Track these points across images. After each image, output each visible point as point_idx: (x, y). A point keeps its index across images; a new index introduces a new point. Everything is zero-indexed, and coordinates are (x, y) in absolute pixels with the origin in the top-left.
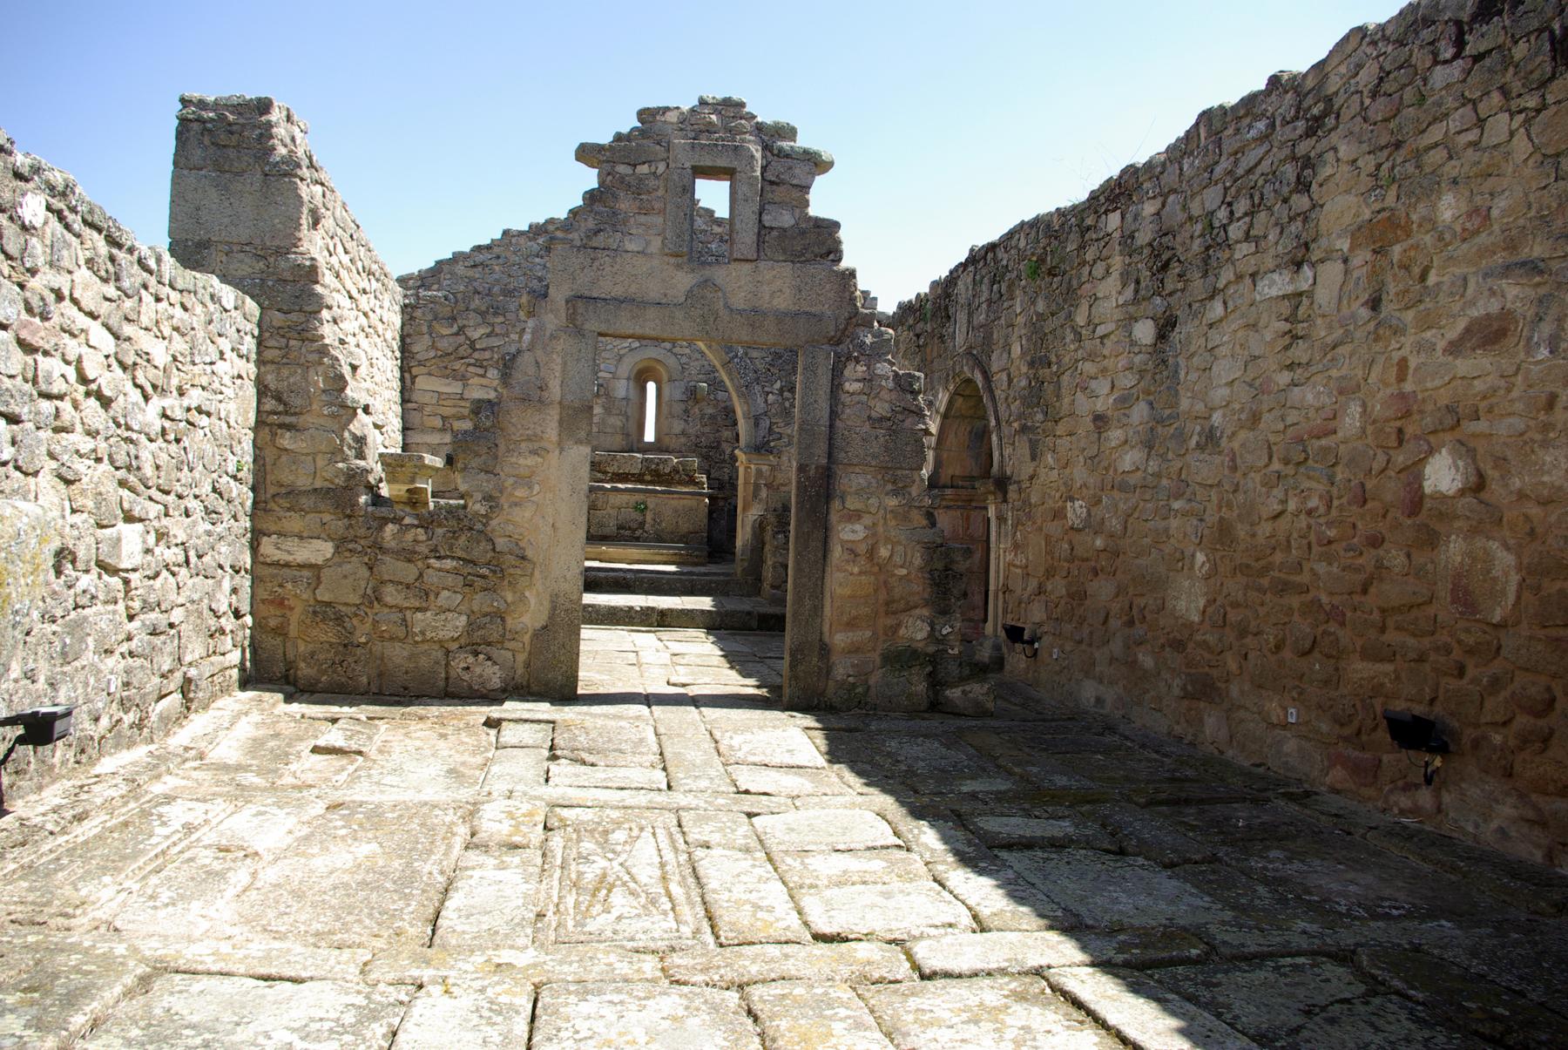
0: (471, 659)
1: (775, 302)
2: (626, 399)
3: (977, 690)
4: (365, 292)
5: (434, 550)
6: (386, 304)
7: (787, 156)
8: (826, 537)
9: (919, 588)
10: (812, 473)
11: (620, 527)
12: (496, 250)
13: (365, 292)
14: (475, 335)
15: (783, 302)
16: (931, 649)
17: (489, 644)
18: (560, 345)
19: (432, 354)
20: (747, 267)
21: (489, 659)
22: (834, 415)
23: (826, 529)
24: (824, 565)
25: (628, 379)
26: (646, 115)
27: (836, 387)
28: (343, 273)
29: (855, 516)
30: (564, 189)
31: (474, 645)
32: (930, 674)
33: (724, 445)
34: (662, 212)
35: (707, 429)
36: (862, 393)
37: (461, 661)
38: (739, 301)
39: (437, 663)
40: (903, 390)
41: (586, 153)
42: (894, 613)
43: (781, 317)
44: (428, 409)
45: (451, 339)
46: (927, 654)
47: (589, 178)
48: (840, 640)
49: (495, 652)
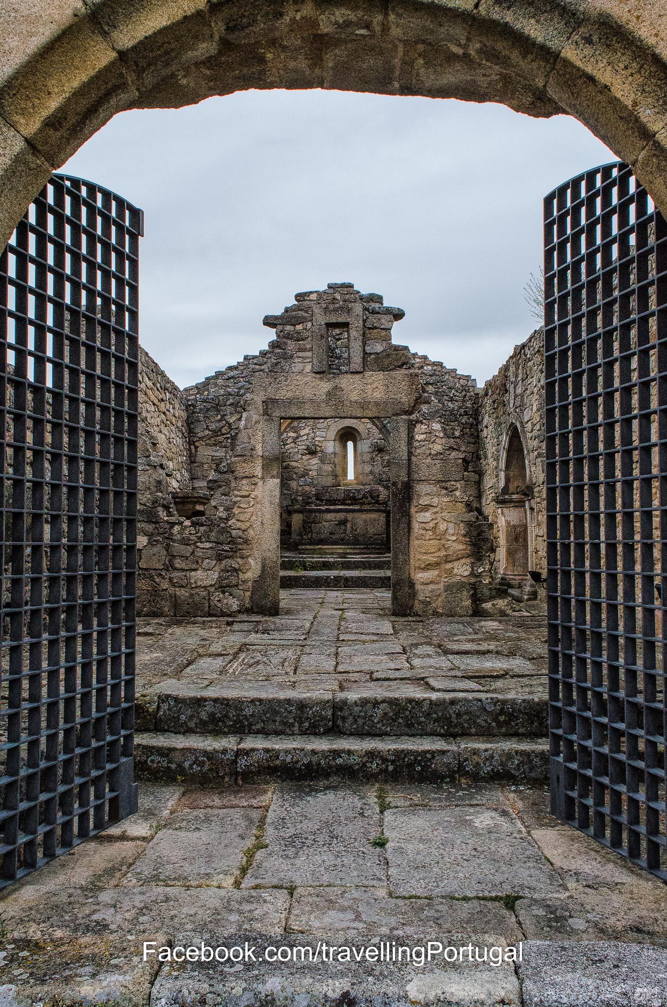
0: (221, 596)
1: (374, 395)
2: (335, 454)
3: (501, 603)
4: (162, 400)
6: (177, 406)
8: (410, 521)
10: (399, 486)
13: (162, 400)
15: (378, 395)
16: (473, 580)
17: (231, 587)
18: (260, 426)
20: (357, 377)
21: (231, 595)
22: (410, 454)
23: (408, 516)
24: (409, 536)
25: (334, 440)
26: (300, 297)
27: (411, 439)
28: (150, 393)
29: (426, 508)
30: (263, 339)
31: (223, 587)
32: (472, 595)
34: (311, 350)
36: (425, 440)
37: (217, 596)
38: (354, 397)
39: (204, 598)
40: (448, 437)
41: (269, 322)
43: (377, 404)
46: (470, 584)
47: (271, 334)
48: (420, 576)
49: (235, 591)
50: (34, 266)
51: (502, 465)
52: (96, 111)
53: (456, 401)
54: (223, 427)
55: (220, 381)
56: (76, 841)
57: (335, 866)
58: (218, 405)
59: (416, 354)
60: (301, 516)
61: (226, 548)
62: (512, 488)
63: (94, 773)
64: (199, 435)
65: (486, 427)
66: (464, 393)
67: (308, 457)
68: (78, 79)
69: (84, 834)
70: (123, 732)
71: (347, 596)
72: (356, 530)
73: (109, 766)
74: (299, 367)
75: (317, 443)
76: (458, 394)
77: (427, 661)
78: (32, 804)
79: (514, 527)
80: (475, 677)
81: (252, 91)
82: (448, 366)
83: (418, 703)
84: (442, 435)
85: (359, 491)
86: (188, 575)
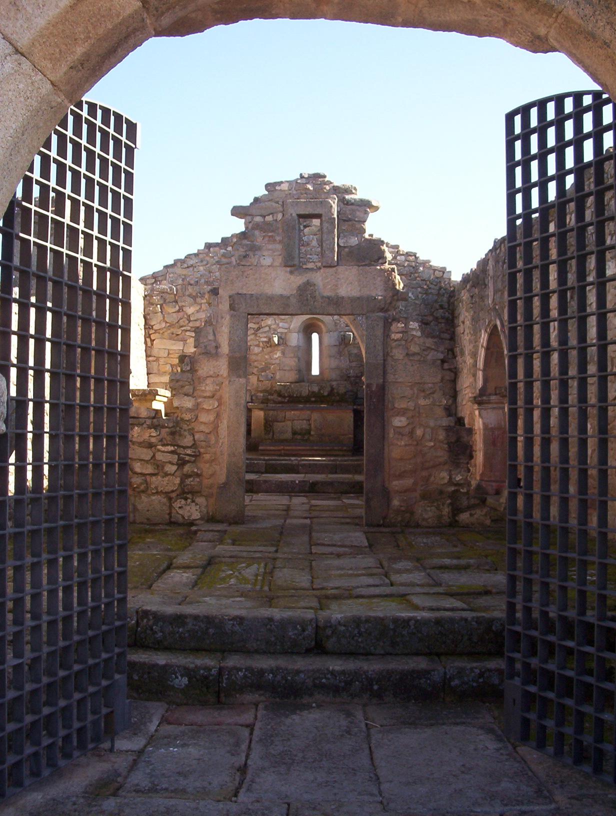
0: (183, 502)
2: (298, 347)
5: (161, 440)
7: (352, 204)
9: (442, 455)
11: (294, 433)
12: (201, 256)
19: (163, 325)
25: (299, 332)
26: (269, 186)
35: (354, 364)
41: (237, 212)
42: (427, 469)
47: (238, 226)
48: (396, 484)
50: (38, 187)
51: (481, 364)
52: (115, 51)
53: (431, 293)
56: (76, 753)
57: (327, 782)
61: (189, 452)
62: (490, 390)
63: (91, 689)
65: (463, 323)
68: (103, 26)
69: (82, 746)
70: (117, 650)
71: (314, 502)
73: (104, 683)
74: (267, 261)
77: (408, 576)
78: (36, 717)
79: (492, 429)
80: (462, 594)
81: (257, 21)
82: (422, 257)
83: (406, 622)
84: (419, 334)
86: (148, 480)
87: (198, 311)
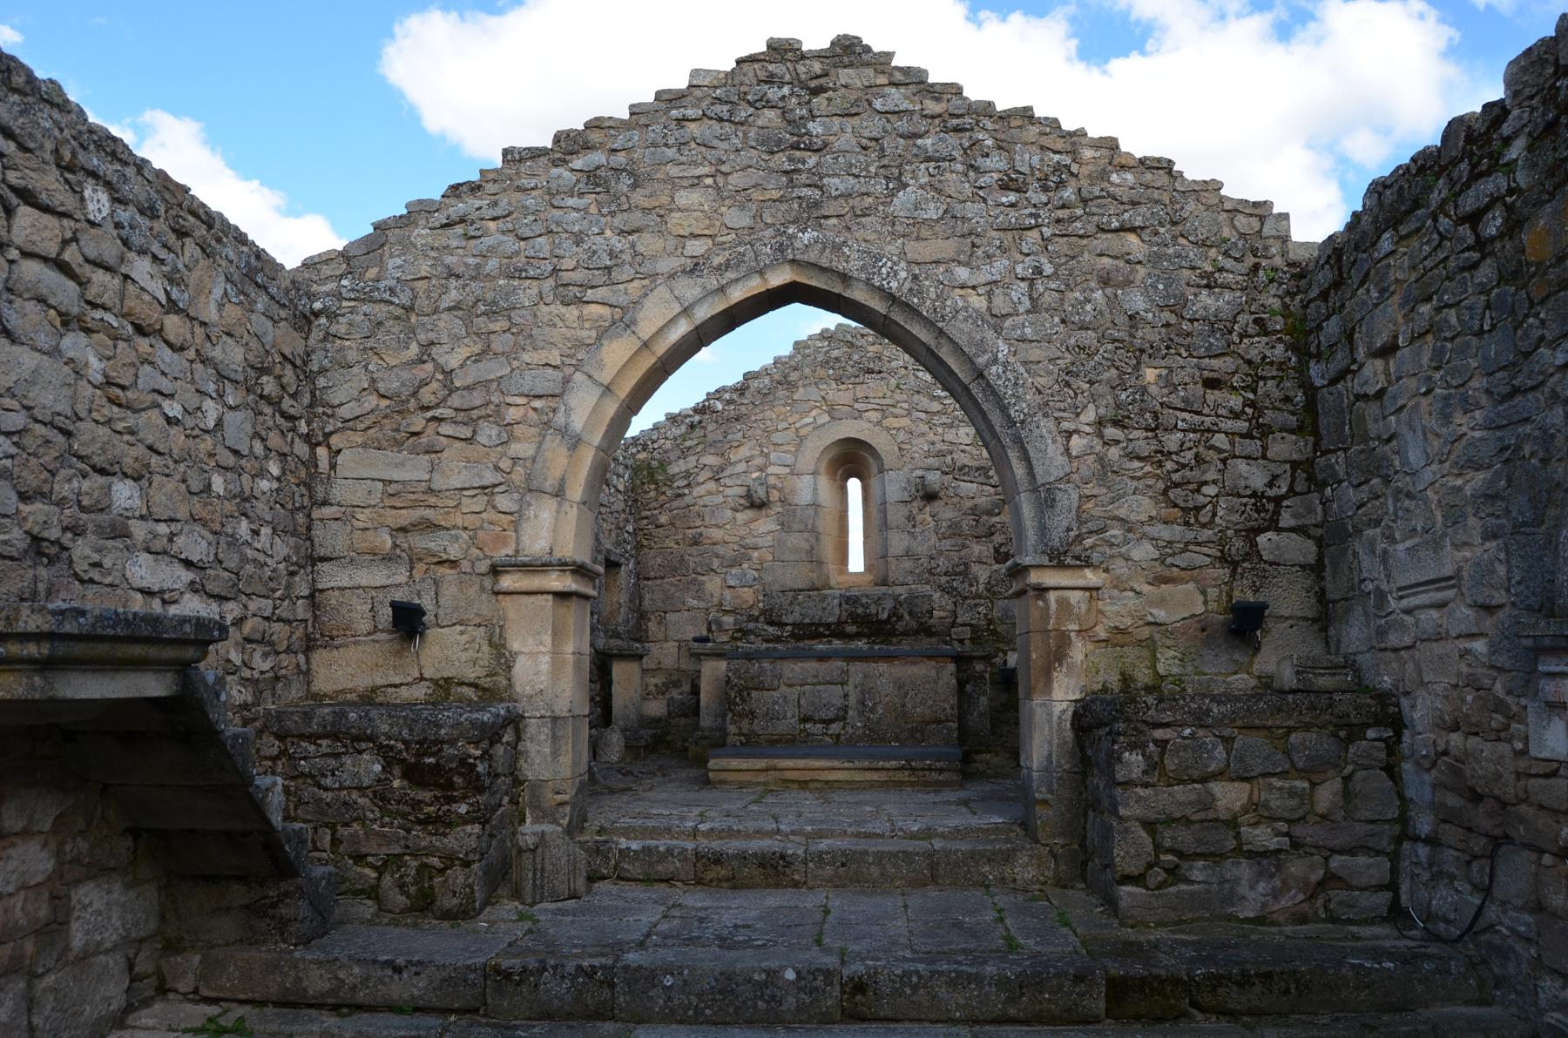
2: (815, 505)
14: (453, 362)
33: (975, 568)
44: (363, 516)
45: (405, 375)
54: (424, 383)
55: (421, 235)
58: (409, 309)
59: (1081, 133)
60: (723, 665)
64: (345, 412)
66: (1250, 260)
67: (750, 513)
72: (872, 710)
75: (772, 480)
76: (1229, 263)
82: (1193, 170)
85: (879, 600)
87: (478, 358)
